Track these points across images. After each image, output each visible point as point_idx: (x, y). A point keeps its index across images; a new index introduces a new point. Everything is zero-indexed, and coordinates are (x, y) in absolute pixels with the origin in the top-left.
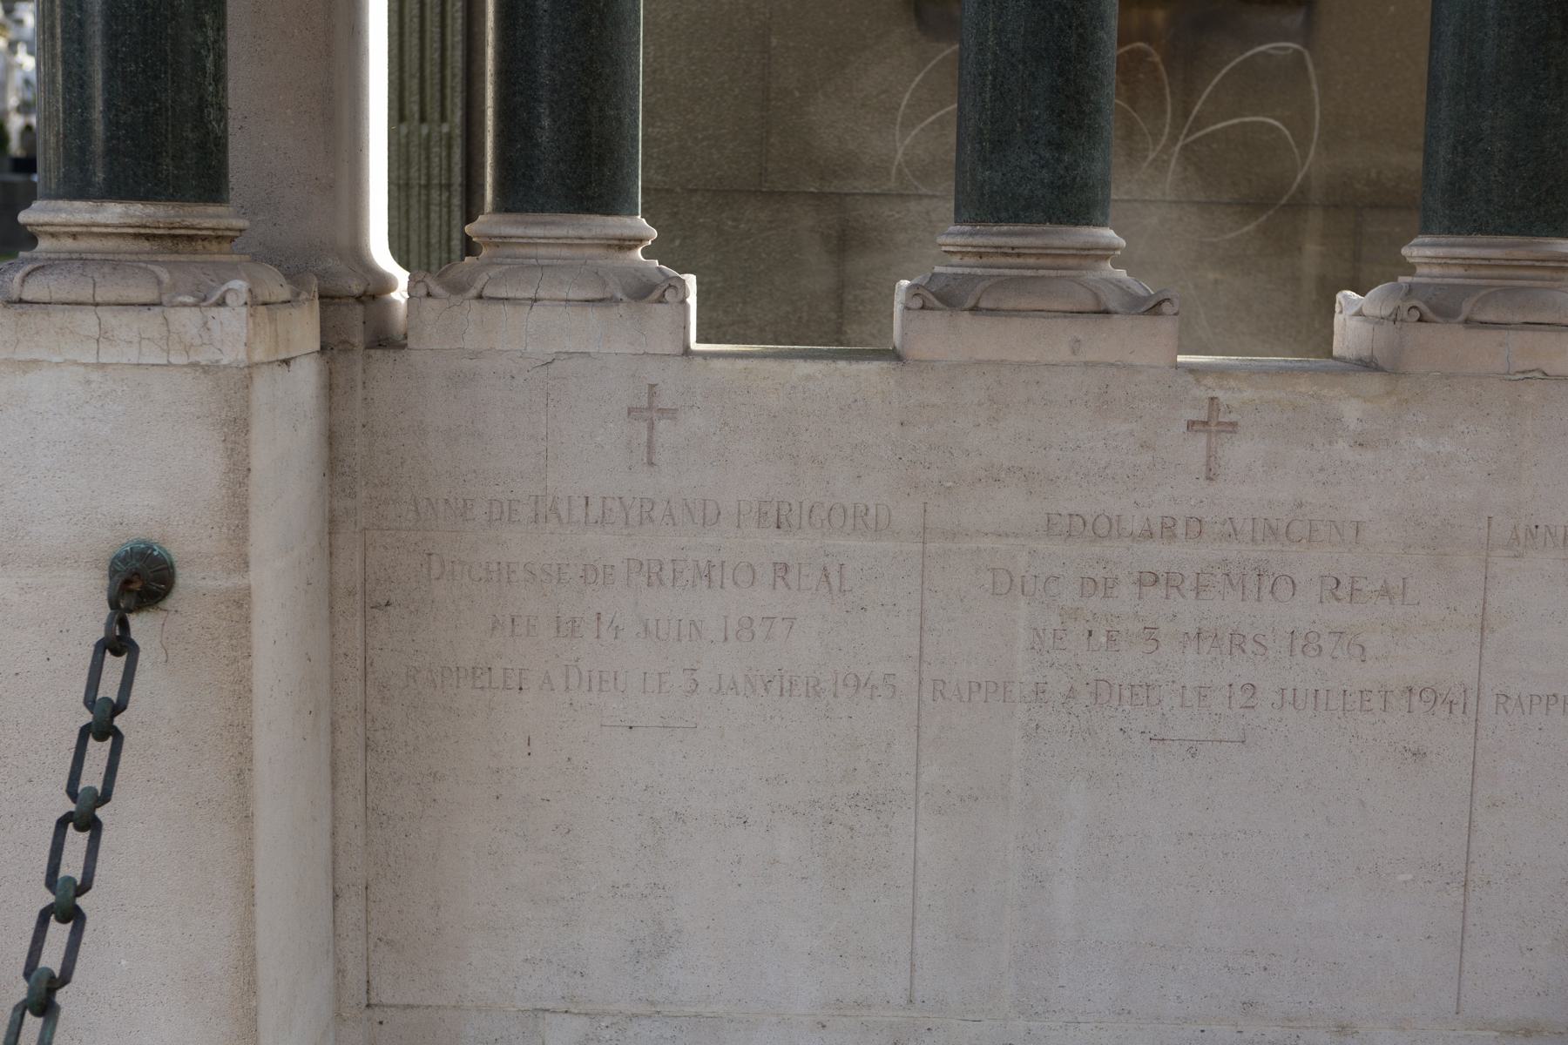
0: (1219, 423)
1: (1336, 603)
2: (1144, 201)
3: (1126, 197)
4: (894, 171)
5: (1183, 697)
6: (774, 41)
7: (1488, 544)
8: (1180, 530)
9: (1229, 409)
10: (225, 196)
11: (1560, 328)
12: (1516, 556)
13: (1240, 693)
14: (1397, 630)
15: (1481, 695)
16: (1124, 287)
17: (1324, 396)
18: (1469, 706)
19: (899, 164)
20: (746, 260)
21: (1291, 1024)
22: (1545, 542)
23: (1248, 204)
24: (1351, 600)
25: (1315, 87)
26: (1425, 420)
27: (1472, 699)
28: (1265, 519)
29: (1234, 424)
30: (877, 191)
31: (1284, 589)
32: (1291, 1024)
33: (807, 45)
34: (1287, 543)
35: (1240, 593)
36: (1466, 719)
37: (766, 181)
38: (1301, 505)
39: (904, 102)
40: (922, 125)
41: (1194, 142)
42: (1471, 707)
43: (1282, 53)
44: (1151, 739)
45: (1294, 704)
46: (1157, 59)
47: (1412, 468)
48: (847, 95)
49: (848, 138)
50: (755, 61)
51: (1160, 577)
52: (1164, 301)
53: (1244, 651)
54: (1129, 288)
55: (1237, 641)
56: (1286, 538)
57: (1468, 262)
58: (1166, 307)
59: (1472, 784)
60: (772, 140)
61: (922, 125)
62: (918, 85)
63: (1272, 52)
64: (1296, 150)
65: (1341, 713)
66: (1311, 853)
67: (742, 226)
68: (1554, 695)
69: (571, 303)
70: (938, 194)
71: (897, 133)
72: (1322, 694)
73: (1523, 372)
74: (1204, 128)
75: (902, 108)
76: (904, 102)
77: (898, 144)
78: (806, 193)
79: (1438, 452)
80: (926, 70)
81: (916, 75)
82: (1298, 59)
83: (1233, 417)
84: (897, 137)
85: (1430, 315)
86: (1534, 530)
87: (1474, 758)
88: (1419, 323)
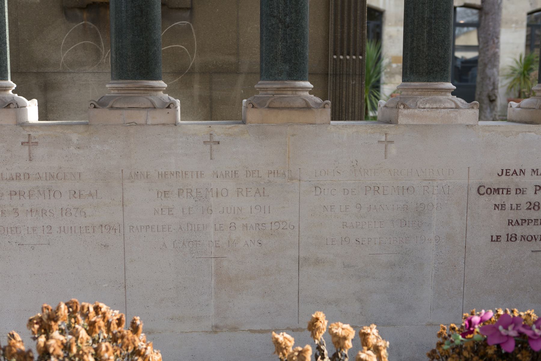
0: (32, 143)
1: (75, 199)
4: (61, 65)
5: (28, 231)
6: (19, 23)
7: (122, 178)
8: (22, 177)
9: (35, 138)
11: (140, 109)
12: (132, 182)
13: (46, 229)
14: (95, 206)
15: (125, 227)
16: (162, 99)
17: (65, 133)
19: (62, 62)
22: (141, 177)
23: (175, 73)
24: (80, 198)
25: (194, 35)
26: (99, 139)
27: (122, 228)
28: (50, 173)
29: (37, 143)
30: (56, 71)
31: (57, 195)
33: (30, 25)
34: (57, 180)
35: (43, 197)
36: (120, 235)
37: (19, 69)
38: (61, 168)
39: (63, 43)
40: (69, 50)
42: (122, 230)
43: (183, 25)
44: (19, 244)
45: (64, 232)
47: (95, 155)
48: (44, 40)
50: (13, 30)
51: (17, 192)
52: (11, 103)
53: (46, 215)
54: (164, 99)
55: (44, 212)
56: (57, 179)
57: (118, 88)
58: (11, 106)
59: (124, 255)
60: (21, 55)
61: (69, 50)
62: (67, 37)
64: (190, 55)
65: (80, 234)
66: (74, 279)
70: (75, 72)
71: (61, 52)
72: (73, 228)
73: (129, 123)
75: (62, 44)
76: (63, 43)
77: (62, 56)
78: (33, 72)
79: (104, 150)
80: (69, 32)
81: (66, 34)
82: (189, 27)
83: (36, 140)
84: (61, 54)
85: (97, 106)
87: (124, 246)
88: (94, 109)
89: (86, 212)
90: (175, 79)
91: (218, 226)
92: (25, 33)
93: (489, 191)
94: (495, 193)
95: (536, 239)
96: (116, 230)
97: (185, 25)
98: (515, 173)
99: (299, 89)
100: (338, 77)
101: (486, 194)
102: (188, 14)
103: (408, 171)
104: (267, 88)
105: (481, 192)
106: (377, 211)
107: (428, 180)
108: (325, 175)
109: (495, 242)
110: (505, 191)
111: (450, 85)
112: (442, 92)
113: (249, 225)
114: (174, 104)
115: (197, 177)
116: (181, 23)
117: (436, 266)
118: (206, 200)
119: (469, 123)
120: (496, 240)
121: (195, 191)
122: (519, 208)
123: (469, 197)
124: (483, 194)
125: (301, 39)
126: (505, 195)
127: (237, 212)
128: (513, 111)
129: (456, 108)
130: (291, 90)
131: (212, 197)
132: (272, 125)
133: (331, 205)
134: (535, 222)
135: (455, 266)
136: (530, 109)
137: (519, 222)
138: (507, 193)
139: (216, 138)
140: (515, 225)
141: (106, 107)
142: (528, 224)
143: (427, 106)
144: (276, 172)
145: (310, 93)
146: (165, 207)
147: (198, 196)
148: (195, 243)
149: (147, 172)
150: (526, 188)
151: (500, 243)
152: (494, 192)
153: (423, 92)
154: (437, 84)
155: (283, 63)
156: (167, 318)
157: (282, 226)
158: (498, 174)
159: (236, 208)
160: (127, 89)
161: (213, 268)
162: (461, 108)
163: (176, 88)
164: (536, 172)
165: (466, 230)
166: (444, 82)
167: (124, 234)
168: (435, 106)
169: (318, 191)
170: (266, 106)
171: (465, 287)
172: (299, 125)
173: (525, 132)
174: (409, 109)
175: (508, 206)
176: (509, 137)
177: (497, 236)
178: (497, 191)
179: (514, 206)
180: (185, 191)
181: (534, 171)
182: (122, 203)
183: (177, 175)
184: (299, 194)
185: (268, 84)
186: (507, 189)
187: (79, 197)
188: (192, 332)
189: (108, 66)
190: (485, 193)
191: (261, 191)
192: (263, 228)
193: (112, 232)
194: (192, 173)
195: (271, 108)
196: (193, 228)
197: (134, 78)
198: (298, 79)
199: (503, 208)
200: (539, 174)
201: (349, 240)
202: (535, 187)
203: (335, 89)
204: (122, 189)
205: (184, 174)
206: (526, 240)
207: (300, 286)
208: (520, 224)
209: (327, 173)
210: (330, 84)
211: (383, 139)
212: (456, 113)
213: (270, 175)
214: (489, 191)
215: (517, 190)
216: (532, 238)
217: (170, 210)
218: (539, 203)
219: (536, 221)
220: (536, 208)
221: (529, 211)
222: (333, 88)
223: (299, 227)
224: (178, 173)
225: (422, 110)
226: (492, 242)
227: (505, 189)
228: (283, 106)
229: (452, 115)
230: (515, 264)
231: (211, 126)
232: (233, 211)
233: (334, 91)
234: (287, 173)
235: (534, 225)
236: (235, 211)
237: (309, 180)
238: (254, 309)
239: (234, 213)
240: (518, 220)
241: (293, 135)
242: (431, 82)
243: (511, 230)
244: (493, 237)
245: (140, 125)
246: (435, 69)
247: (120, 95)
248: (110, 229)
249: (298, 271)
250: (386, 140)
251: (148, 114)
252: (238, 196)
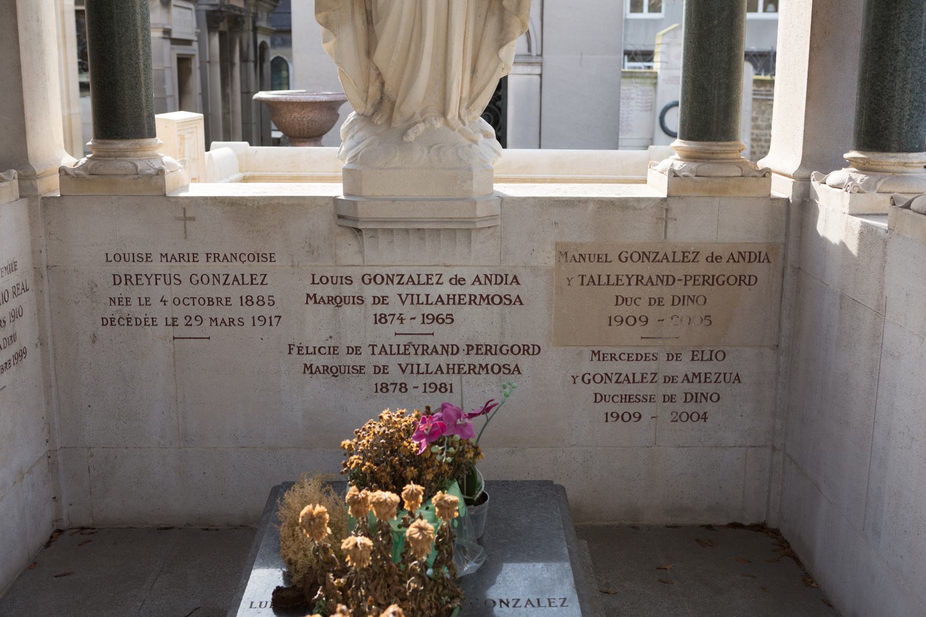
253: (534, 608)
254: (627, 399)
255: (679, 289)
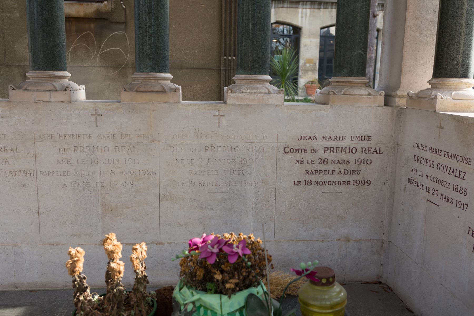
1: (1, 152)
2: (92, 66)
3: (88, 66)
6: (5, 31)
10: (469, 77)
12: (41, 141)
18: (34, 174)
20: (3, 80)
21: (3, 245)
24: (5, 152)
25: (128, 41)
27: (35, 173)
32: (3, 245)
36: (34, 177)
37: (6, 62)
41: (102, 53)
46: (93, 35)
49: (24, 53)
52: (66, 88)
60: (7, 53)
63: (118, 33)
67: (2, 72)
68: (328, 171)
69: (155, 92)
73: (38, 101)
74: (104, 50)
78: (15, 65)
85: (15, 88)
86: (44, 135)
87: (37, 185)
89: (9, 161)
90: (115, 71)
91: (102, 172)
92: (10, 38)
93: (292, 151)
94: (296, 152)
95: (325, 184)
96: (31, 175)
97: (121, 34)
98: (310, 138)
99: (160, 79)
100: (227, 72)
101: (290, 153)
102: (123, 26)
103: (234, 136)
104: (138, 78)
105: (287, 151)
106: (213, 163)
107: (249, 142)
108: (176, 138)
109: (296, 186)
110: (303, 151)
111: (268, 77)
112: (260, 82)
113: (124, 172)
114: (178, 89)
115: (87, 139)
116: (119, 33)
117: (255, 201)
118: (94, 154)
119: (277, 104)
120: (297, 184)
121: (86, 148)
122: (313, 163)
123: (278, 154)
124: (288, 153)
125: (161, 44)
126: (303, 153)
127: (115, 163)
128: (317, 95)
129: (269, 93)
130: (154, 79)
131: (98, 152)
132: (139, 103)
133: (181, 159)
134: (324, 172)
135: (269, 202)
136: (325, 94)
137: (313, 172)
138: (305, 152)
139: (99, 112)
140: (310, 174)
141: (21, 89)
142: (320, 174)
143: (248, 91)
144: (143, 135)
145: (171, 81)
146: (65, 159)
147: (88, 151)
148: (87, 183)
149: (52, 135)
150: (318, 149)
151: (300, 186)
152: (295, 151)
153: (247, 82)
154: (256, 76)
155: (148, 60)
156: (69, 235)
157: (147, 173)
158: (298, 139)
159: (115, 160)
160: (38, 77)
161: (100, 201)
162: (272, 93)
163: (116, 78)
164: (325, 138)
165: (276, 177)
166: (262, 75)
167: (37, 177)
168: (253, 91)
169: (172, 150)
170: (134, 90)
171: (276, 216)
172: (157, 103)
173: (317, 110)
174: (235, 94)
175: (305, 161)
176: (306, 113)
177: (298, 181)
178: (298, 150)
179: (310, 161)
180: (79, 148)
181: (323, 137)
182: (35, 155)
183: (73, 137)
184: (158, 151)
185: (138, 75)
186: (305, 149)
187: (4, 151)
188: (86, 244)
189: (68, 61)
190: (289, 152)
191: (132, 149)
192: (134, 174)
193: (28, 175)
194: (83, 136)
195: (139, 91)
196: (85, 174)
197: (43, 69)
198: (159, 72)
199: (302, 163)
200: (327, 140)
201: (194, 183)
202: (324, 148)
203: (225, 80)
204: (34, 146)
205: (78, 136)
206: (318, 184)
207: (160, 214)
208: (314, 174)
209: (178, 136)
210: (222, 76)
211: (217, 114)
212: (268, 97)
213: (138, 138)
214: (292, 150)
215: (311, 150)
216: (323, 183)
217: (68, 161)
218: (327, 160)
219: (325, 172)
220: (325, 163)
221: (320, 164)
222: (224, 79)
223: (159, 174)
224: (73, 136)
225: (244, 94)
226: (295, 186)
227: (303, 149)
228: (146, 90)
229: (265, 98)
230: (311, 201)
231: (96, 103)
232: (112, 162)
233: (225, 81)
234: (150, 137)
235: (324, 174)
236: (114, 162)
237: (166, 141)
238: (129, 229)
239: (114, 164)
240: (312, 171)
241: (154, 111)
242: (252, 75)
243: (308, 177)
244: (295, 182)
245: (46, 102)
246: (255, 66)
247: (33, 81)
248: (27, 173)
249: (159, 204)
250: (219, 114)
251: (51, 94)
252: (116, 152)
253: (334, 154)
254: (446, 169)
255: (359, 155)
